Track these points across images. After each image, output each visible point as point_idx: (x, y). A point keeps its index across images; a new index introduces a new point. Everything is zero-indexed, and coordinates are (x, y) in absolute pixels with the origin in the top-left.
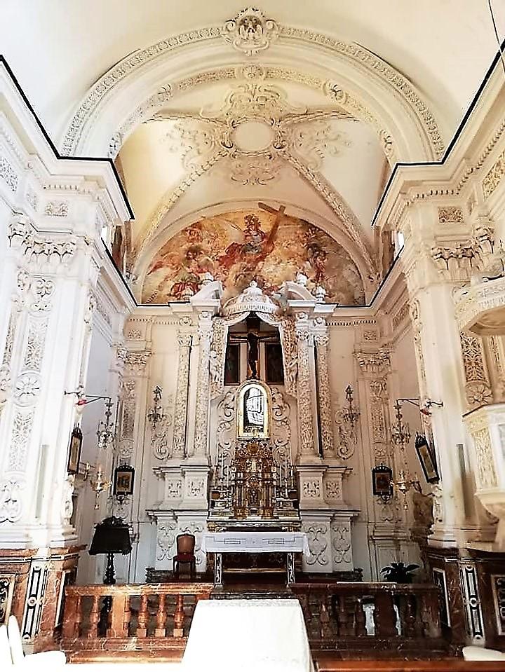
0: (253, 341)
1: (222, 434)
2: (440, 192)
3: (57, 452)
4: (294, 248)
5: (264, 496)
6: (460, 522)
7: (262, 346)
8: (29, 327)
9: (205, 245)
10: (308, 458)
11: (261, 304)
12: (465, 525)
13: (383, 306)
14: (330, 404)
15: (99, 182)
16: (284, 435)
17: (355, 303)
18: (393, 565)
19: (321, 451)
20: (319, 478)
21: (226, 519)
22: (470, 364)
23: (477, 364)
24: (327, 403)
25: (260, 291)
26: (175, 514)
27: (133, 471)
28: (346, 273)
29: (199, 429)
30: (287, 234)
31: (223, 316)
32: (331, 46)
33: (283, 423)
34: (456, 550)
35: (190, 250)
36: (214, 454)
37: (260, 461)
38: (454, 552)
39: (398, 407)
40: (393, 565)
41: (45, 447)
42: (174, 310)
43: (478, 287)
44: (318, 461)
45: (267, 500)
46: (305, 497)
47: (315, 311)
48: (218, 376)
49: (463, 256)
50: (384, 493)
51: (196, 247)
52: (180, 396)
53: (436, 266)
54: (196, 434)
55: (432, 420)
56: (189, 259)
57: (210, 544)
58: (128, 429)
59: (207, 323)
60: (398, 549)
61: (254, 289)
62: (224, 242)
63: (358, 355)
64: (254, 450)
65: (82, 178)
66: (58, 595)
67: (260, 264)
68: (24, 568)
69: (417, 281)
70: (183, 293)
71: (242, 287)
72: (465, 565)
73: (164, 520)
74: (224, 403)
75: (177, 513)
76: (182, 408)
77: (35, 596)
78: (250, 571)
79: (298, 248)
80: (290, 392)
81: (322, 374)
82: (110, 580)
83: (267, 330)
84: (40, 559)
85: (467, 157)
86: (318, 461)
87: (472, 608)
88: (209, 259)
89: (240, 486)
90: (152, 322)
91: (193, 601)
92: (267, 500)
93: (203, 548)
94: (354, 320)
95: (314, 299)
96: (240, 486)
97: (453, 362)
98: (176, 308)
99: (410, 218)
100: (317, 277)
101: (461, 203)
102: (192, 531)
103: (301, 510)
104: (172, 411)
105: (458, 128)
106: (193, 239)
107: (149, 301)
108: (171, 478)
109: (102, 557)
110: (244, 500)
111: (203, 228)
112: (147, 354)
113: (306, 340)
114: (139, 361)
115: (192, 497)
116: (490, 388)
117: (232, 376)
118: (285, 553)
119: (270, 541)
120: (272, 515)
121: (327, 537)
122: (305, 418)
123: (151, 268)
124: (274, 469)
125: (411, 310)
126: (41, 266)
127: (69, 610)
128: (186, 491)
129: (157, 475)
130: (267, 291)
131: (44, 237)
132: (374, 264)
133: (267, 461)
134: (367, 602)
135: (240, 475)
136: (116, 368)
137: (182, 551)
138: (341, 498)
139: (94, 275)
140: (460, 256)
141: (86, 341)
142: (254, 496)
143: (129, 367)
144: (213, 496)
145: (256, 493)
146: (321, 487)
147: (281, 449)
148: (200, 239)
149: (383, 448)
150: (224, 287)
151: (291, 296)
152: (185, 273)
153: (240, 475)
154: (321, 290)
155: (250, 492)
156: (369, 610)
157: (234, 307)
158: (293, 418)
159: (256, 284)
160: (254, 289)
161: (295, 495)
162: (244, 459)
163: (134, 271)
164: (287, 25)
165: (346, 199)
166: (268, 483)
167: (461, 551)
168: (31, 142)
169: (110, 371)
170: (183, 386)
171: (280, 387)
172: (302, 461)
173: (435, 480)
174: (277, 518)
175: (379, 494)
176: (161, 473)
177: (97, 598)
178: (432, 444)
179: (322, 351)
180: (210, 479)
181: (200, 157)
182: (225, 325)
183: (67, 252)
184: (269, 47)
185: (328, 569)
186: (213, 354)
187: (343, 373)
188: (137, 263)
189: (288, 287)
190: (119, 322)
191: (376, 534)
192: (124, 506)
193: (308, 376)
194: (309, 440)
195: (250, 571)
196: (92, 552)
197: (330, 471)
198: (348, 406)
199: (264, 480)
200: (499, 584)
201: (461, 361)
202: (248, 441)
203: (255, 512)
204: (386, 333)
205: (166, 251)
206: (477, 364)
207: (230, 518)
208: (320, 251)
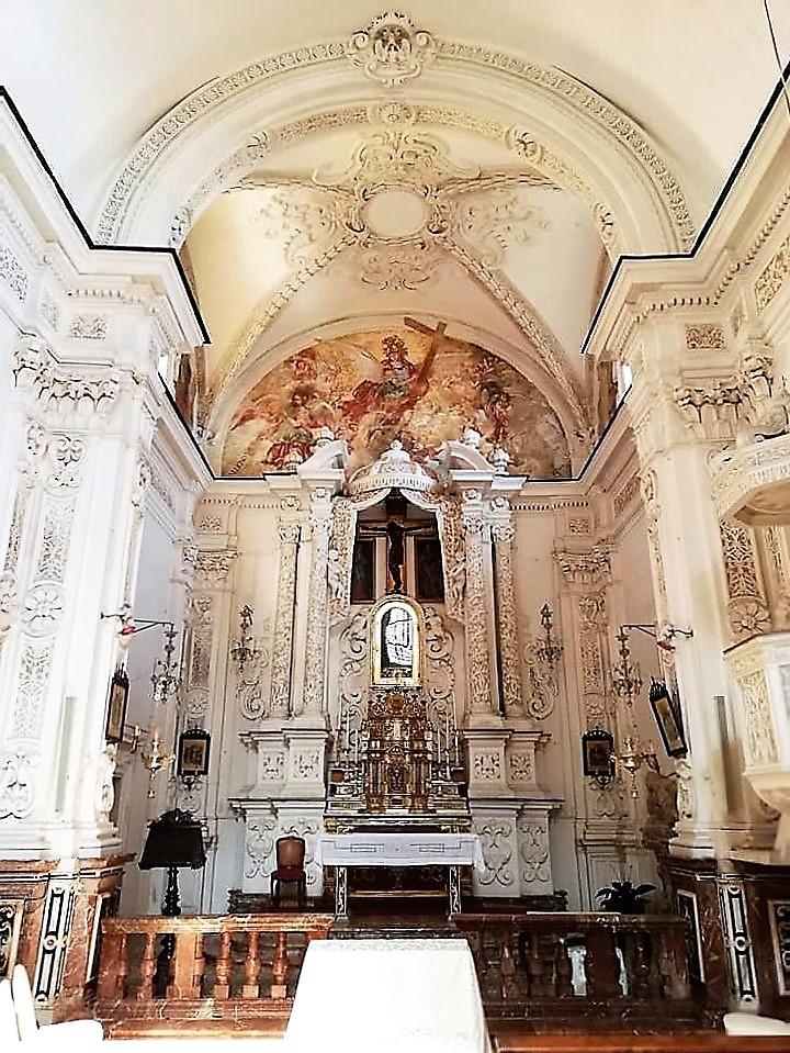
0: (396, 535)
1: (348, 680)
2: (688, 301)
3: (89, 709)
4: (460, 389)
5: (413, 777)
6: (719, 818)
7: (410, 542)
8: (45, 512)
9: (321, 384)
10: (482, 718)
11: (409, 476)
12: (727, 822)
13: (600, 479)
14: (517, 633)
15: (155, 286)
16: (445, 681)
17: (556, 474)
18: (615, 885)
19: (503, 707)
20: (499, 748)
21: (354, 813)
22: (736, 570)
23: (746, 570)
24: (511, 631)
25: (406, 456)
26: (273, 805)
27: (208, 738)
28: (541, 428)
29: (312, 672)
30: (448, 367)
31: (348, 496)
32: (518, 72)
33: (443, 663)
34: (713, 861)
35: (298, 391)
36: (335, 711)
37: (407, 722)
38: (710, 865)
39: (623, 638)
40: (615, 885)
41: (70, 700)
42: (273, 486)
43: (747, 449)
44: (497, 722)
45: (418, 784)
46: (477, 779)
47: (493, 487)
48: (341, 588)
49: (725, 401)
50: (600, 773)
51: (307, 387)
52: (281, 621)
53: (682, 417)
54: (306, 680)
55: (677, 659)
56: (296, 405)
57: (328, 852)
58: (200, 672)
59: (323, 507)
60: (623, 861)
61: (397, 452)
62: (350, 380)
63: (560, 556)
64: (397, 705)
65: (129, 279)
66: (91, 933)
67: (407, 413)
68: (38, 890)
69: (652, 440)
70: (287, 459)
71: (379, 450)
72: (728, 886)
73: (256, 815)
74: (351, 631)
75: (277, 804)
76: (285, 640)
77: (55, 934)
78: (391, 894)
79: (466, 389)
80: (453, 614)
81: (504, 586)
82: (171, 909)
83: (417, 516)
84: (63, 877)
85: (730, 246)
86: (497, 722)
87: (738, 953)
88: (328, 406)
89: (376, 762)
90: (238, 504)
91: (302, 942)
92: (418, 784)
93: (317, 858)
94: (554, 502)
95: (491, 469)
96: (376, 762)
97: (709, 567)
98: (276, 482)
99: (641, 342)
100: (496, 434)
101: (721, 318)
102: (300, 833)
103: (471, 799)
104: (269, 645)
105: (717, 200)
106: (302, 374)
107: (234, 472)
108: (268, 749)
109: (159, 873)
110: (382, 783)
111: (318, 357)
112: (230, 554)
113: (479, 533)
114: (218, 566)
115: (301, 779)
116: (766, 608)
117: (362, 590)
118: (446, 867)
119: (422, 847)
120: (425, 807)
121: (512, 841)
122: (477, 655)
123: (237, 421)
124: (429, 736)
125: (643, 487)
126: (65, 417)
127: (108, 957)
128: (291, 769)
129: (246, 745)
130: (418, 456)
131: (69, 371)
132: (585, 414)
133: (417, 723)
134: (573, 943)
135: (376, 744)
136: (181, 576)
137: (284, 863)
138: (534, 781)
139: (148, 430)
140: (720, 401)
141: (134, 534)
142: (397, 778)
143: (201, 575)
144: (333, 777)
145: (401, 773)
146: (502, 762)
147: (440, 704)
148: (313, 374)
149: (598, 701)
150: (351, 449)
151: (454, 464)
152: (289, 427)
153: (376, 744)
154: (502, 455)
155: (391, 772)
156: (577, 956)
157: (366, 482)
158: (458, 655)
159: (400, 445)
160: (397, 452)
161: (461, 775)
162: (381, 719)
163: (210, 424)
164: (450, 40)
165: (541, 311)
166: (419, 756)
167: (720, 863)
168: (48, 222)
169: (173, 581)
170: (286, 605)
171: (437, 607)
172: (473, 722)
173: (680, 752)
174: (434, 811)
175: (593, 774)
176: (252, 741)
177: (151, 937)
178: (676, 695)
179: (503, 550)
180: (328, 750)
181: (313, 246)
182: (352, 509)
183: (104, 395)
184: (420, 73)
185: (514, 892)
186: (333, 554)
187: (537, 585)
188: (214, 413)
189: (450, 450)
190: (186, 504)
191: (588, 837)
192: (193, 793)
193: (482, 590)
194: (484, 690)
195: (391, 894)
196: (144, 865)
197: (516, 738)
198: (544, 636)
199: (412, 752)
200: (781, 915)
201: (722, 566)
202: (388, 691)
203: (399, 802)
204: (604, 521)
205: (259, 394)
206: (746, 570)
207: (360, 811)
208: (501, 393)
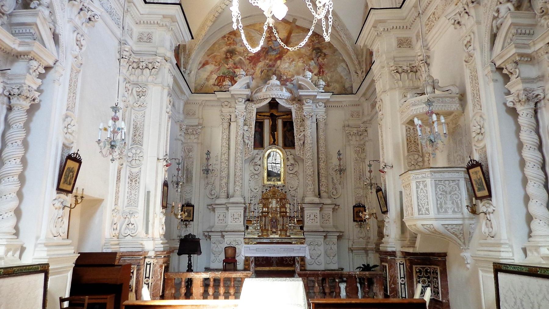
0: (273, 118)
1: (253, 183)
2: (398, 27)
3: (155, 196)
5: (281, 223)
6: (398, 237)
7: (280, 123)
8: (133, 117)
10: (311, 198)
11: (280, 93)
12: (401, 238)
13: (364, 94)
14: (326, 162)
15: (173, 19)
17: (346, 91)
18: (363, 265)
19: (319, 194)
20: (317, 211)
21: (256, 237)
22: (411, 141)
23: (415, 142)
24: (324, 161)
25: (278, 82)
26: (222, 234)
27: (193, 206)
28: (339, 69)
29: (237, 179)
31: (252, 101)
34: (394, 252)
35: (229, 51)
36: (248, 195)
38: (393, 254)
39: (370, 166)
40: (363, 265)
41: (149, 192)
43: (412, 99)
44: (317, 200)
45: (283, 225)
46: (308, 223)
47: (318, 97)
48: (250, 143)
49: (411, 71)
50: (360, 221)
52: (223, 157)
53: (393, 77)
54: (235, 182)
55: (386, 177)
56: (227, 58)
57: (245, 252)
58: (189, 179)
59: (241, 106)
60: (367, 255)
61: (274, 81)
63: (347, 128)
64: (274, 193)
65: (162, 16)
66: (161, 278)
67: (279, 62)
68: (142, 262)
69: (381, 87)
70: (224, 83)
71: (266, 79)
72: (399, 260)
73: (215, 237)
74: (254, 161)
75: (224, 233)
76: (225, 165)
77: (149, 278)
78: (272, 268)
81: (321, 142)
82: (190, 270)
83: (283, 110)
84: (150, 257)
86: (317, 200)
87: (401, 284)
90: (203, 105)
93: (243, 253)
94: (344, 104)
95: (317, 89)
96: (265, 216)
97: (400, 140)
98: (220, 95)
99: (379, 43)
100: (319, 72)
101: (412, 34)
102: (234, 244)
104: (218, 167)
106: (230, 43)
107: (200, 90)
108: (219, 211)
109: (185, 257)
112: (200, 127)
114: (195, 133)
117: (259, 143)
118: (294, 257)
119: (285, 250)
120: (286, 235)
121: (322, 248)
122: (309, 172)
123: (201, 65)
124: (288, 206)
125: (377, 106)
126: (138, 77)
128: (229, 219)
129: (210, 209)
130: (284, 82)
132: (359, 63)
133: (283, 200)
134: (343, 281)
135: (265, 209)
136: (179, 137)
137: (228, 256)
138: (331, 224)
139: (170, 81)
140: (409, 71)
141: (168, 123)
144: (248, 223)
146: (318, 218)
147: (293, 193)
149: (361, 192)
150: (253, 79)
151: (300, 87)
152: (224, 68)
153: (265, 209)
155: (272, 220)
156: (343, 286)
157: (260, 95)
159: (275, 77)
160: (274, 81)
161: (301, 221)
162: (268, 199)
163: (189, 67)
166: (284, 214)
167: (397, 253)
169: (176, 139)
170: (225, 150)
171: (292, 151)
172: (307, 200)
173: (385, 212)
174: (290, 236)
175: (356, 221)
176: (212, 208)
177: (184, 280)
178: (385, 190)
179: (321, 126)
180: (245, 212)
182: (254, 108)
183: (154, 68)
186: (246, 128)
187: (336, 141)
188: (190, 62)
189: (298, 81)
190: (180, 105)
191: (353, 246)
193: (312, 143)
194: (311, 187)
195: (272, 268)
196: (179, 254)
197: (325, 206)
198: (338, 164)
199: (281, 212)
200: (418, 271)
201: (405, 140)
202: (270, 187)
203: (275, 232)
204: (366, 113)
205: (210, 53)
206: (415, 142)
207: (259, 236)
208: (321, 52)
